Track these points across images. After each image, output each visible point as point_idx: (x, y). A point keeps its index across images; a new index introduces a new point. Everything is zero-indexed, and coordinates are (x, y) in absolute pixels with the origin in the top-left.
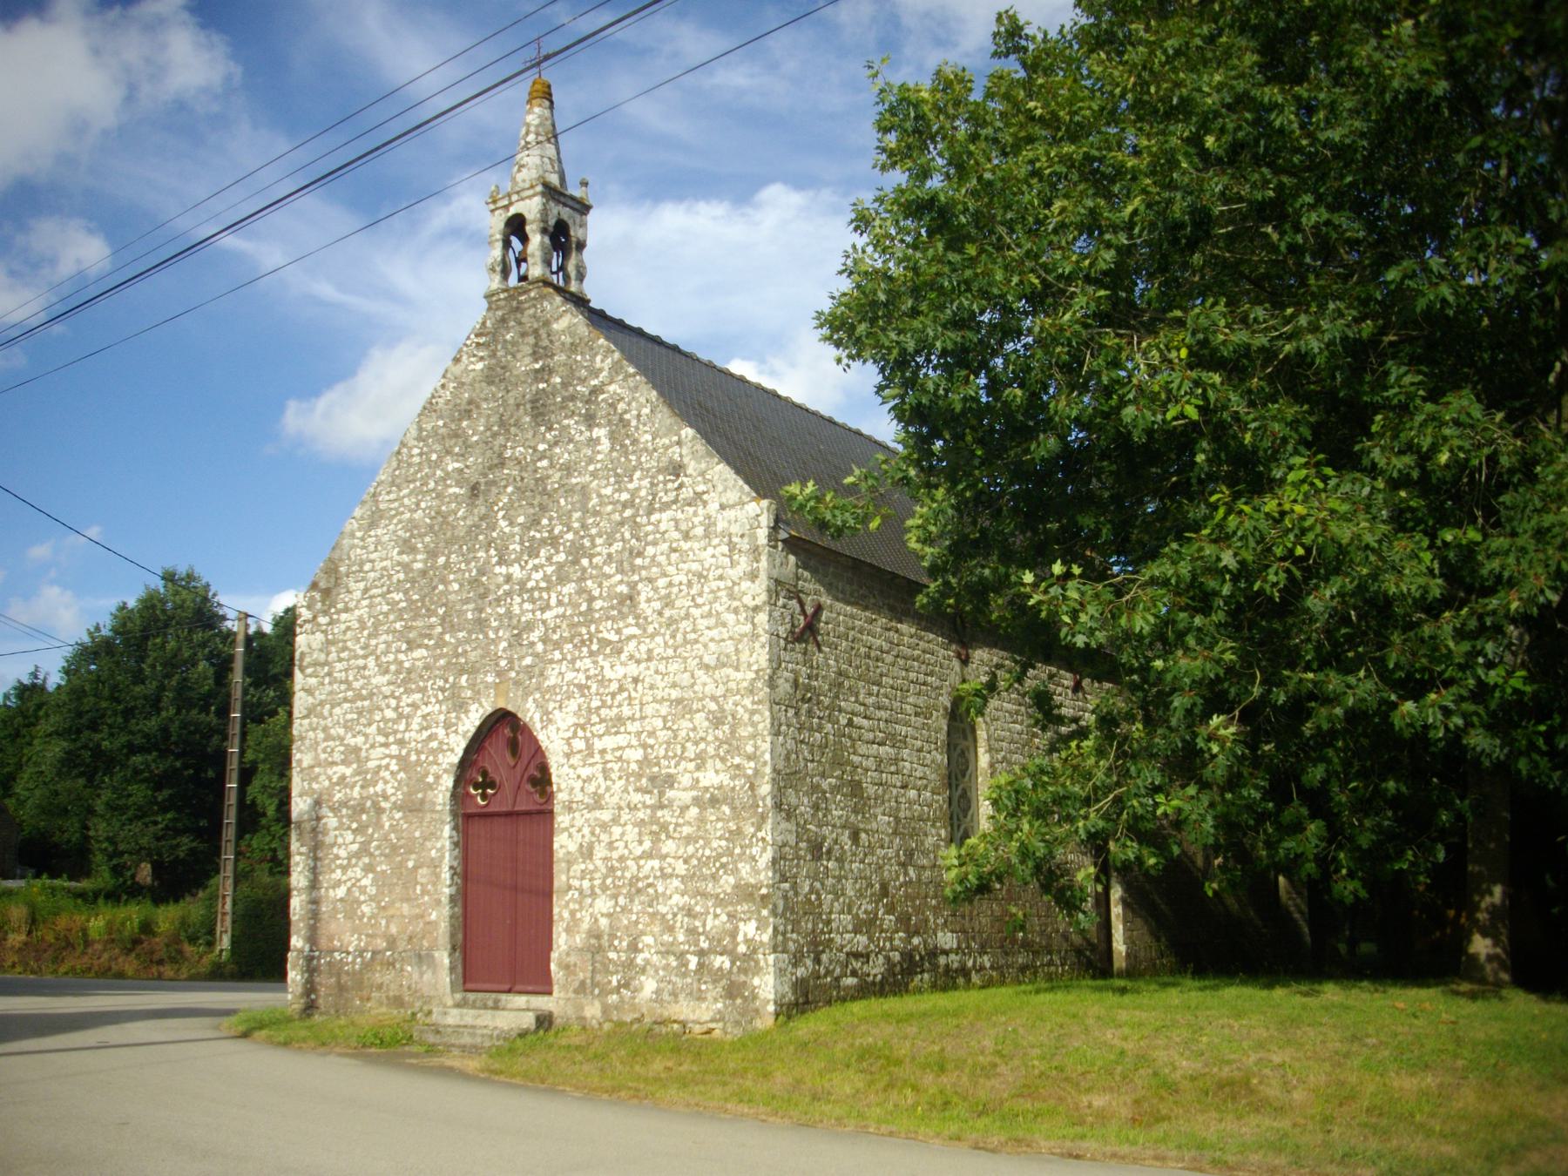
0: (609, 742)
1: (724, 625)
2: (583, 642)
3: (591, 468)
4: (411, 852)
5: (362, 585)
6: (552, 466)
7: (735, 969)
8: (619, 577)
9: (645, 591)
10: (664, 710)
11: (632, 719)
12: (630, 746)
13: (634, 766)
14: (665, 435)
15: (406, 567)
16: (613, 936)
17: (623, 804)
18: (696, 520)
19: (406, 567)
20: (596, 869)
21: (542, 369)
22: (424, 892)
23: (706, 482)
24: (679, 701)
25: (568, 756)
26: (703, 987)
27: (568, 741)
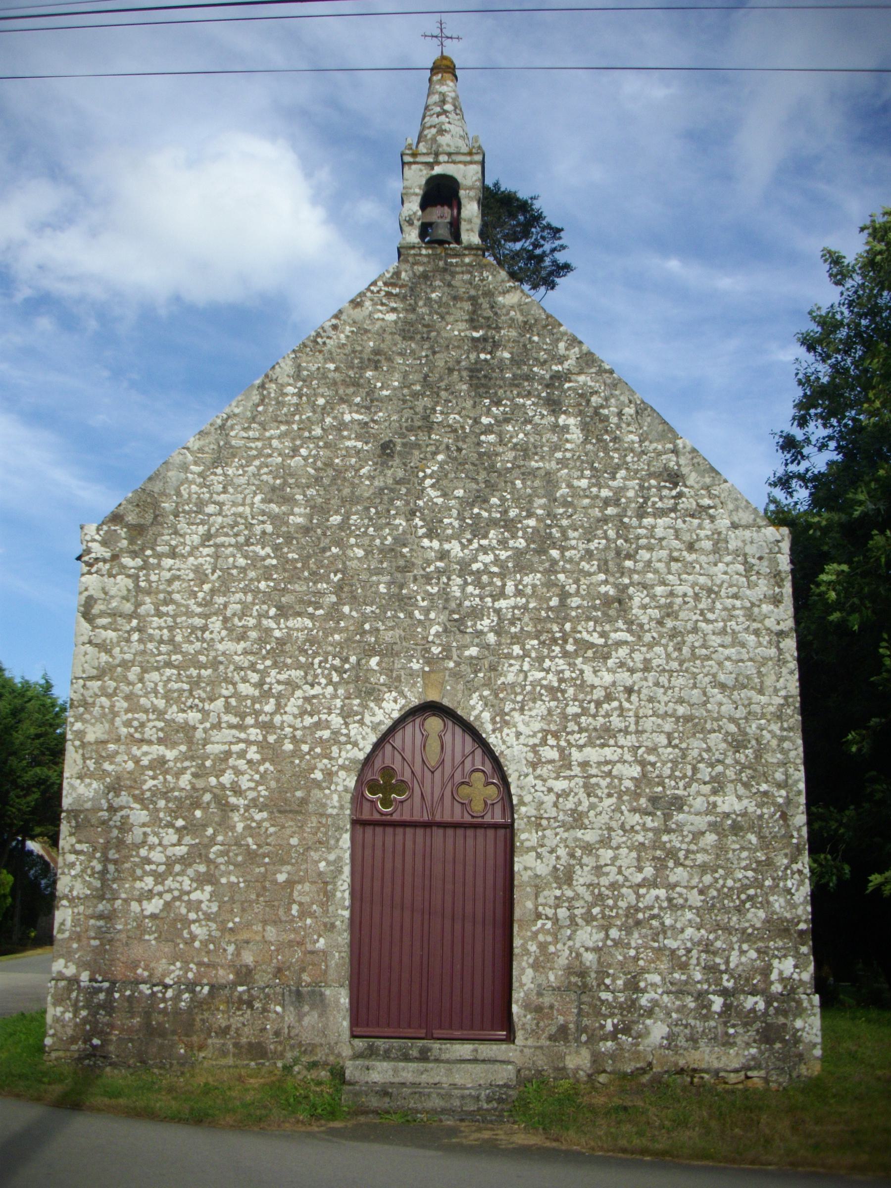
0: (593, 754)
1: (743, 645)
2: (554, 641)
3: (559, 455)
4: (283, 862)
5: (201, 529)
6: (501, 442)
7: (771, 1011)
8: (602, 577)
9: (638, 598)
10: (668, 726)
11: (626, 732)
13: (628, 784)
14: (658, 441)
15: (275, 519)
16: (602, 973)
17: (614, 824)
18: (702, 533)
19: (275, 519)
20: (577, 897)
21: (484, 339)
22: (303, 914)
23: (711, 496)
24: (688, 719)
25: (534, 765)
26: (731, 1031)
27: (534, 748)
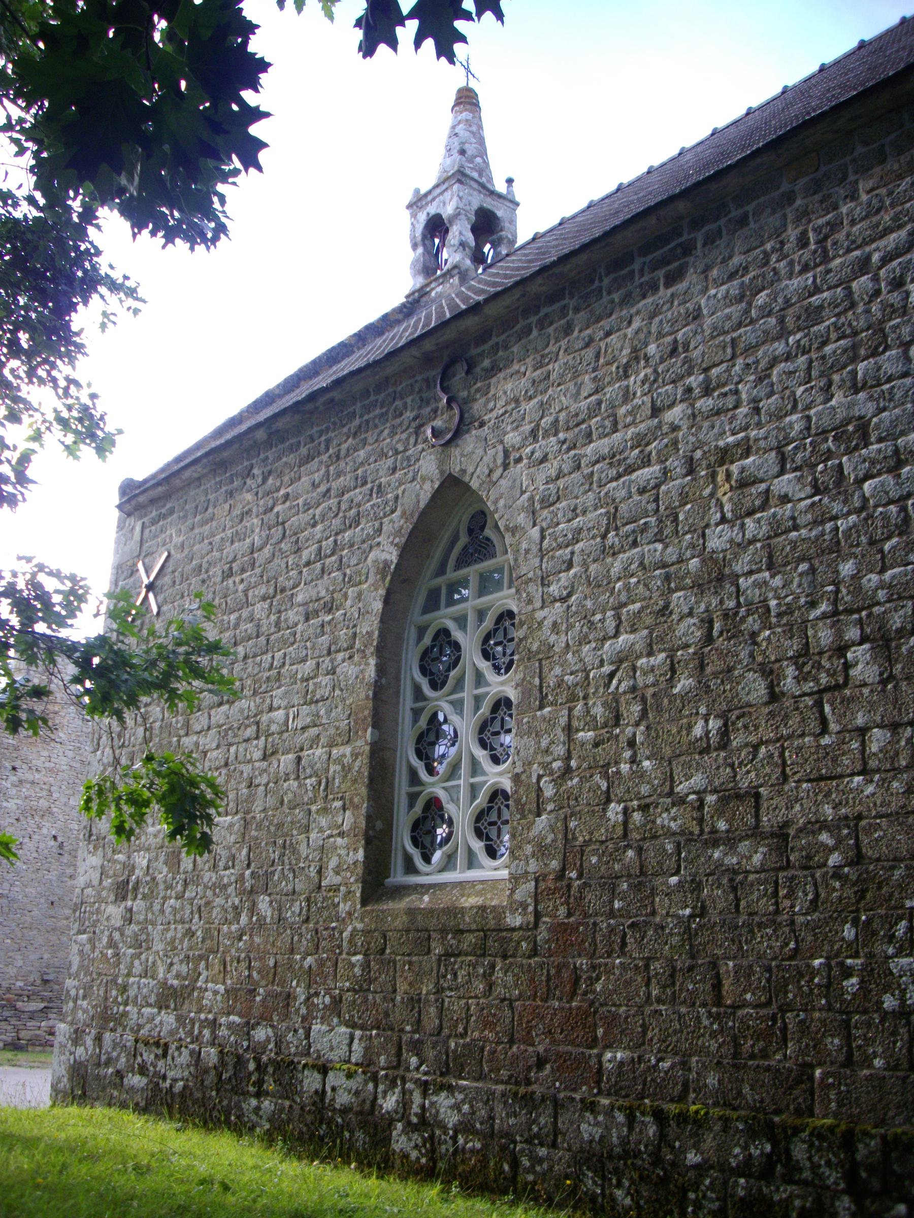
12: (570, 710)
